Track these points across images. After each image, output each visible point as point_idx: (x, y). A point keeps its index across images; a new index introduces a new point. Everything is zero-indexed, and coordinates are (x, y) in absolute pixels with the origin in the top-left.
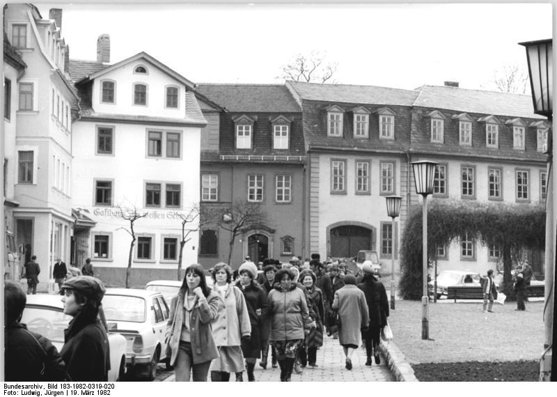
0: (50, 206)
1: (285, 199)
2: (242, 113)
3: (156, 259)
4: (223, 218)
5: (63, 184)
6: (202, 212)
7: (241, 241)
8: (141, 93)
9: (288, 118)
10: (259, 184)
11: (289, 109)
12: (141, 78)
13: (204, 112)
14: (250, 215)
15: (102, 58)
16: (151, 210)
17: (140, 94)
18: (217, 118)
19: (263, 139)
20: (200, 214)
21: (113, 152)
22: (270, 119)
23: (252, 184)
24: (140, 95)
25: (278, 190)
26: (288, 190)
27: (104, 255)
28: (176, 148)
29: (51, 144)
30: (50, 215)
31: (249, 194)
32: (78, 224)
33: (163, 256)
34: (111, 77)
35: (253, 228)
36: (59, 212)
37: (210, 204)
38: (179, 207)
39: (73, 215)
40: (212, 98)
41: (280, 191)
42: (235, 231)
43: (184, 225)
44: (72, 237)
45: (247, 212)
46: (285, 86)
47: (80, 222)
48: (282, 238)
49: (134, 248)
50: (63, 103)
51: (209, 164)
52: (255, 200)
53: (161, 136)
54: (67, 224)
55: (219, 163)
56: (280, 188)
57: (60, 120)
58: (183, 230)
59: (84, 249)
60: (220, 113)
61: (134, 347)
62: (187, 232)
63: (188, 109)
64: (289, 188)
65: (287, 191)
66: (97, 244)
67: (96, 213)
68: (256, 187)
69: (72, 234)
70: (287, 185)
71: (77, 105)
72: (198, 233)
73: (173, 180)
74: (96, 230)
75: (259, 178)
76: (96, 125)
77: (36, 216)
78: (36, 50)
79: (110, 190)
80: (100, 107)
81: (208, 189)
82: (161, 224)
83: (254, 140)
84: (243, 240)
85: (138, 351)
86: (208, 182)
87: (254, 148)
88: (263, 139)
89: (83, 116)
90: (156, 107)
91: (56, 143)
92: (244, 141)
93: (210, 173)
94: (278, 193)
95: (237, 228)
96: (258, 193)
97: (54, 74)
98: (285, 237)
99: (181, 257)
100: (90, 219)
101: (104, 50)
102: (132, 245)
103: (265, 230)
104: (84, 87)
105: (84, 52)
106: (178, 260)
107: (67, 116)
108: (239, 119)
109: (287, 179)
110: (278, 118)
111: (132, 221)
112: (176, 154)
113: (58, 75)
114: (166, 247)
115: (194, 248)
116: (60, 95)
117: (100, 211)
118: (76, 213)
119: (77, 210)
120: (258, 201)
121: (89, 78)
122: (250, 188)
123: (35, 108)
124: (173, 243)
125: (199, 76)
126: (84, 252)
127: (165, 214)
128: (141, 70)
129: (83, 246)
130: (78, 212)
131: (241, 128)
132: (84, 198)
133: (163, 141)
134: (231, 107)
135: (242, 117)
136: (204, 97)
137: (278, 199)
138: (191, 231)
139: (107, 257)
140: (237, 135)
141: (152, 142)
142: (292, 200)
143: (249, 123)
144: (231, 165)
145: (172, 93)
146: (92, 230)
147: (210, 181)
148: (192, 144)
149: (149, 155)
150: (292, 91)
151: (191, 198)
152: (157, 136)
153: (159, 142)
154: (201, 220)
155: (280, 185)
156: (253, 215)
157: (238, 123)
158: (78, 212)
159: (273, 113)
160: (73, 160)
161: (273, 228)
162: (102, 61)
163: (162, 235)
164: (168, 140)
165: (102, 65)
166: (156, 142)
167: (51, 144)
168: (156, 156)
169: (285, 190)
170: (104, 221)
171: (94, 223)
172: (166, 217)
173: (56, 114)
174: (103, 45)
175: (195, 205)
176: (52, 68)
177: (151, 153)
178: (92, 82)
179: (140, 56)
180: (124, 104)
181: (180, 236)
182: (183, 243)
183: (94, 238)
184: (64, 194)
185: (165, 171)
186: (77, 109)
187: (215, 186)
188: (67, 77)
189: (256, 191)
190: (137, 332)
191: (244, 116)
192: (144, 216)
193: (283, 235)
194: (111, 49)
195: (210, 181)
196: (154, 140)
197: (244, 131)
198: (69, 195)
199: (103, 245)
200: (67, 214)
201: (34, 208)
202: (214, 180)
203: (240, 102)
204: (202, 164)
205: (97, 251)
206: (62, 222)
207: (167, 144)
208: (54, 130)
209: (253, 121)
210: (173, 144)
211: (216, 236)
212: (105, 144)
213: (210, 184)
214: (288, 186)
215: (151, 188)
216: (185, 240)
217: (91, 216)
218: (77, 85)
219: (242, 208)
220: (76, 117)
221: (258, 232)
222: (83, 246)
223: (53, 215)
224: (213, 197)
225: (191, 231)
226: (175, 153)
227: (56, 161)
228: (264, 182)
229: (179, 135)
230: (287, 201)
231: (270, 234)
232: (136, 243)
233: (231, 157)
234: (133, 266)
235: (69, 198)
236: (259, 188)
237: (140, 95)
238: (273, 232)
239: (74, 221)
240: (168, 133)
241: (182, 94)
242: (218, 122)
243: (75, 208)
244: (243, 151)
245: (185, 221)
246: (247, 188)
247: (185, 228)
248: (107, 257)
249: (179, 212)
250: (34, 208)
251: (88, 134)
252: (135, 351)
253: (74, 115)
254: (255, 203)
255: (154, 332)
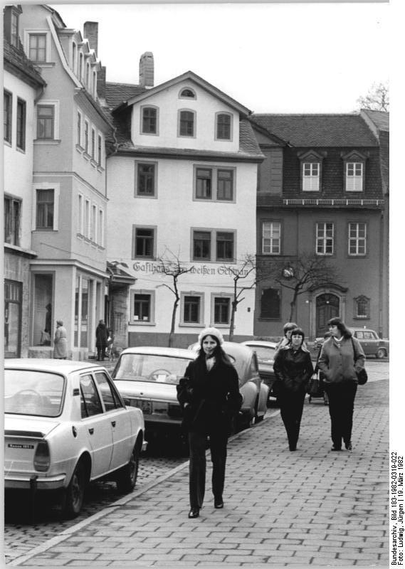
0: (73, 257)
1: (359, 252)
2: (309, 148)
3: (205, 323)
4: (283, 272)
5: (93, 231)
6: (258, 268)
7: (307, 302)
8: (151, 119)
9: (363, 154)
10: (329, 234)
11: (364, 142)
12: (187, 104)
13: (262, 146)
14: (315, 270)
15: (146, 81)
16: (198, 265)
17: (187, 124)
18: (279, 153)
19: (332, 180)
20: (257, 268)
21: (155, 195)
22: (342, 155)
23: (321, 234)
24: (187, 124)
25: (351, 241)
26: (331, 240)
27: (145, 318)
28: (228, 190)
29: (76, 181)
30: (74, 269)
31: (317, 246)
32: (114, 280)
33: (213, 320)
34: (151, 103)
35: (324, 286)
36: (84, 264)
37: (271, 259)
38: (232, 261)
39: (107, 270)
40: (282, 135)
41: (353, 242)
42: (297, 289)
43: (236, 283)
44: (106, 296)
45: (311, 267)
46: (359, 116)
47: (117, 278)
48: (355, 299)
49: (178, 309)
50: (93, 132)
51: (267, 209)
52: (325, 253)
53: (211, 175)
54: (100, 281)
55: (282, 208)
56: (353, 238)
57: (90, 152)
58: (235, 287)
59: (122, 311)
60: (283, 148)
61: (35, 461)
62: (241, 290)
63: (242, 141)
64: (364, 239)
65: (361, 243)
66: (137, 305)
67: (136, 268)
68: (325, 238)
69: (106, 293)
70: (361, 234)
71: (112, 137)
72: (253, 292)
73: (225, 226)
74: (137, 287)
75: (329, 226)
76: (194, 165)
77: (57, 270)
78: (57, 66)
79: (152, 239)
80: (140, 140)
81: (270, 240)
82: (210, 280)
83: (323, 180)
84: (310, 301)
85: (42, 467)
86: (270, 231)
87: (323, 190)
88: (332, 180)
89: (120, 149)
90: (205, 139)
91: (83, 180)
92: (311, 183)
93: (271, 221)
94: (331, 248)
95: (298, 285)
96: (327, 244)
97: (79, 94)
98: (359, 297)
99: (233, 320)
100: (129, 275)
101: (146, 71)
102: (176, 305)
103: (336, 288)
104: (122, 116)
105: (123, 72)
106: (229, 326)
107: (100, 149)
108: (305, 156)
109: (361, 227)
110: (351, 154)
111: (175, 277)
112: (228, 195)
113: (82, 96)
114: (217, 308)
115: (249, 310)
116: (88, 121)
117: (140, 265)
118: (111, 268)
119: (113, 264)
120: (327, 254)
121: (127, 103)
122: (318, 238)
123: (56, 137)
124: (195, 303)
125: (260, 105)
126: (122, 314)
127: (216, 269)
128: (188, 94)
129: (121, 307)
130: (115, 266)
131: (308, 167)
132: (122, 251)
133: (212, 179)
134: (296, 140)
135: (309, 153)
136: (265, 129)
137: (351, 252)
138: (245, 288)
139: (148, 321)
140: (304, 175)
141: (200, 181)
142: (367, 253)
143: (318, 160)
144: (296, 211)
145: (187, 119)
146: (132, 287)
147: (272, 230)
148: (247, 182)
149: (197, 197)
150: (368, 121)
151: (246, 246)
152: (206, 174)
153: (209, 182)
154: (257, 275)
155: (353, 234)
156: (318, 270)
157: (305, 160)
158: (115, 266)
159: (345, 147)
160: (108, 203)
161: (345, 286)
162: (146, 85)
163: (212, 294)
164: (219, 179)
165: (145, 89)
166: (205, 181)
167: (76, 181)
168: (204, 198)
169: (360, 241)
170: (144, 278)
171: (134, 280)
172: (216, 272)
173: (83, 144)
174: (146, 63)
175: (249, 256)
176: (77, 87)
177: (200, 195)
178: (131, 107)
179: (186, 77)
180: (167, 136)
181: (231, 295)
182: (235, 303)
183: (133, 298)
184: (94, 244)
185: (215, 215)
186: (113, 141)
187: (278, 236)
188: (102, 103)
189: (325, 242)
190: (40, 434)
191: (311, 151)
192: (190, 270)
193: (358, 294)
194: (155, 70)
195: (272, 230)
196: (203, 179)
197: (311, 170)
198: (103, 246)
199: (144, 305)
200: (101, 268)
201: (46, 260)
202: (276, 230)
203: (307, 135)
204: (260, 210)
205: (136, 313)
206: (92, 277)
207: (218, 182)
208: (80, 165)
209: (321, 157)
210: (224, 185)
211: (278, 296)
212: (146, 185)
213: (272, 234)
214: (363, 236)
215: (200, 237)
216: (238, 300)
217: (130, 271)
218: (114, 113)
219: (304, 261)
220: (112, 152)
221: (328, 291)
222: (121, 307)
223: (79, 269)
224: (275, 249)
225: (245, 288)
226: (227, 194)
227: (83, 203)
228: (335, 232)
229: (231, 172)
230: (361, 254)
231: (342, 294)
232: (181, 304)
233: (296, 201)
234: (177, 331)
235: (103, 249)
236: (329, 238)
237: (187, 124)
238: (345, 291)
239: (109, 277)
240: (219, 170)
241: (235, 124)
242: (281, 160)
243: (110, 262)
244: (311, 194)
245: (238, 277)
246: (318, 239)
247: (237, 285)
248: (148, 321)
249: (233, 266)
250: (46, 260)
251: (126, 172)
252: (37, 468)
253: (108, 148)
254: (325, 257)
255: (75, 434)
